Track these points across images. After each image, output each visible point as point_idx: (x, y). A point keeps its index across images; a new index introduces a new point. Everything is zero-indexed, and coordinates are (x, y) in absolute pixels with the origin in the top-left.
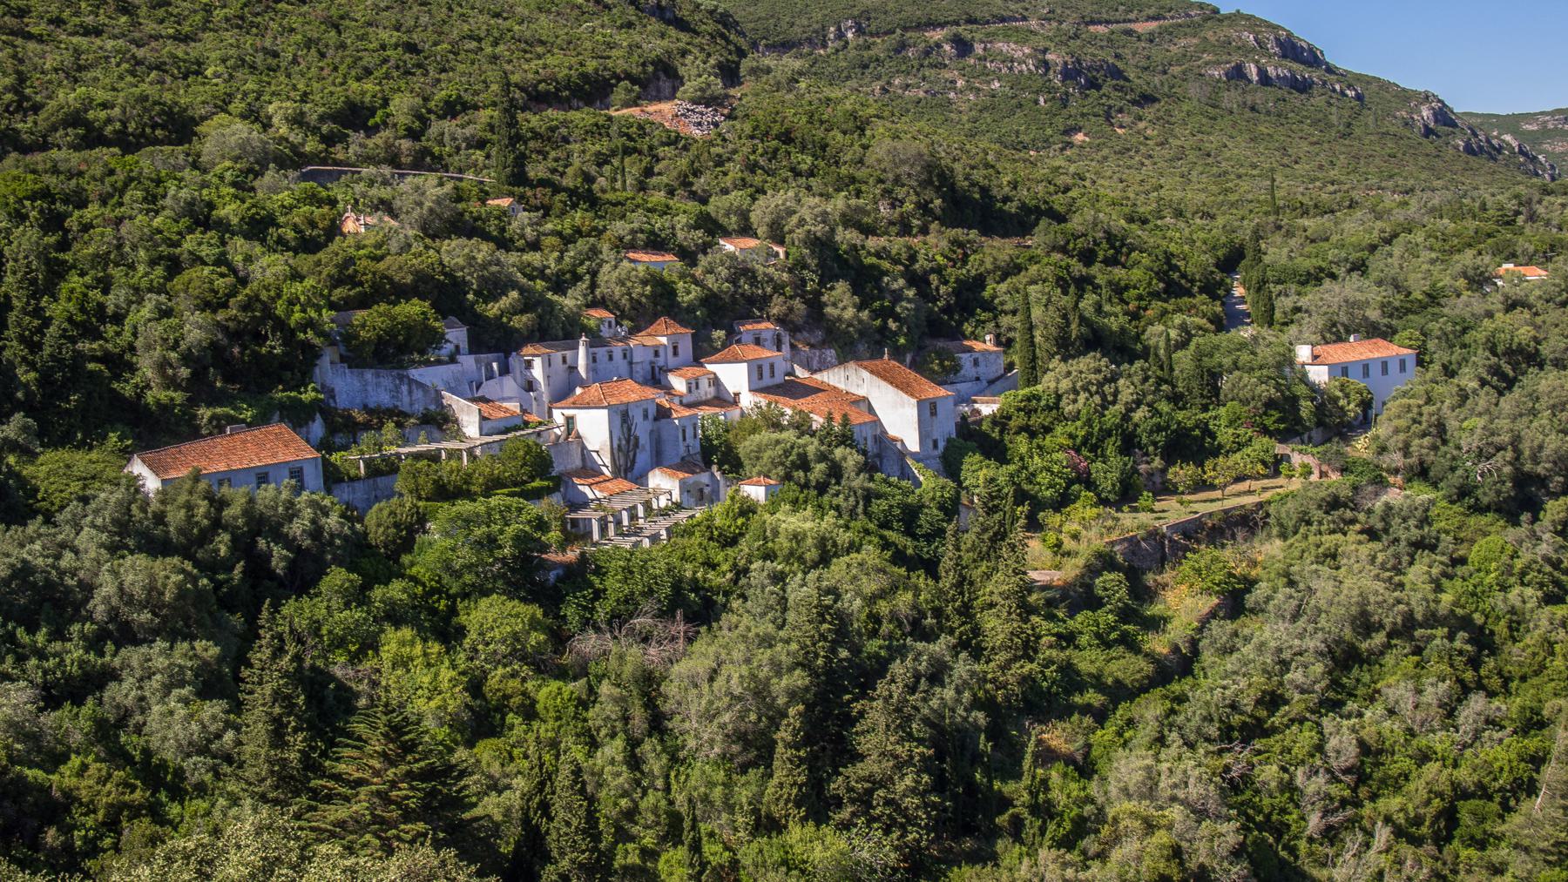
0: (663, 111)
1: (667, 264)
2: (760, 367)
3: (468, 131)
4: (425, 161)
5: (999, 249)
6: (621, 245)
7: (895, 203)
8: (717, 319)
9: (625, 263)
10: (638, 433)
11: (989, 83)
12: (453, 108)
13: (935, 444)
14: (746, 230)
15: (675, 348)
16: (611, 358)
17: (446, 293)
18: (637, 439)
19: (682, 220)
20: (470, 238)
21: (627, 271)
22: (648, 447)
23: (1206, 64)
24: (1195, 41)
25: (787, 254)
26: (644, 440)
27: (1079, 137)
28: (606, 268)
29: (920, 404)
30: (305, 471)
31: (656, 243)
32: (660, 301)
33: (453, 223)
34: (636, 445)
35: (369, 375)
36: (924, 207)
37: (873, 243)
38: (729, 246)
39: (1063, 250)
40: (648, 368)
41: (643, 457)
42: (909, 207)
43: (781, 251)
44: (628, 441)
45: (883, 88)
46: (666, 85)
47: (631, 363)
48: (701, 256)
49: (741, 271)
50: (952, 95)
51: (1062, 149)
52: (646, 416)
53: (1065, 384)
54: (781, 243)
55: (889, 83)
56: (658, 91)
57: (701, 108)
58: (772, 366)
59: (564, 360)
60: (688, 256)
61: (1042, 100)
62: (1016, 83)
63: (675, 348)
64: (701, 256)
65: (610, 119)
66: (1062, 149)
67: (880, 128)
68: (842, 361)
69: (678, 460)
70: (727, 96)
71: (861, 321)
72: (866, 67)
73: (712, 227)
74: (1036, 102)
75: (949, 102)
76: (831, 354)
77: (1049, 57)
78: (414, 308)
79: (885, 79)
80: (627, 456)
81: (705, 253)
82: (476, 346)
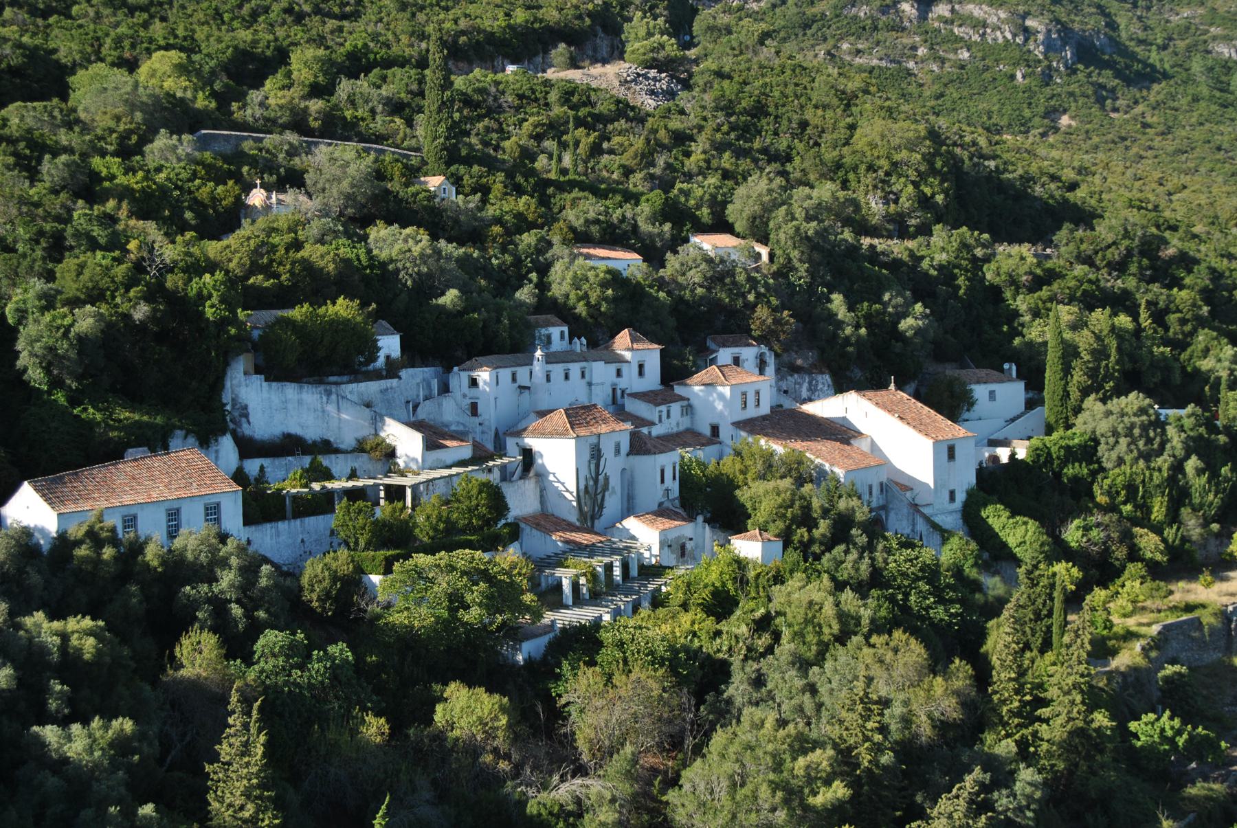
0: (606, 77)
1: (628, 262)
2: (744, 394)
3: (385, 91)
4: (336, 127)
5: (1013, 258)
6: (580, 237)
7: (890, 198)
8: (691, 329)
9: (580, 261)
10: (608, 471)
11: (955, 51)
12: (357, 64)
13: (952, 494)
14: (721, 225)
15: (641, 367)
16: (567, 377)
17: (374, 284)
18: (607, 479)
19: (645, 209)
20: (404, 226)
21: (579, 271)
22: (618, 489)
23: (1214, 38)
24: (1201, 11)
25: (772, 256)
26: (615, 482)
27: (1065, 120)
28: (558, 267)
29: (937, 443)
30: (240, 520)
31: (614, 236)
32: (628, 307)
33: (378, 204)
34: (606, 487)
35: (291, 390)
36: (925, 202)
37: (866, 241)
38: (707, 243)
39: (1088, 261)
40: (610, 391)
41: (612, 503)
42: (905, 203)
43: (764, 251)
44: (596, 481)
45: (829, 53)
46: (603, 43)
47: (590, 384)
48: (669, 255)
49: (720, 272)
50: (911, 65)
51: (1043, 135)
52: (618, 451)
53: (1103, 427)
54: (764, 240)
55: (836, 47)
56: (595, 50)
57: (653, 73)
58: (758, 393)
59: (514, 380)
60: (654, 255)
61: (1019, 75)
62: (988, 53)
63: (641, 367)
64: (669, 255)
65: (547, 83)
66: (1043, 135)
67: (867, 105)
68: (840, 387)
69: (655, 507)
70: (685, 58)
71: (859, 336)
72: (806, 26)
73: (682, 220)
74: (1012, 77)
75: (909, 73)
76: (825, 379)
77: (1030, 23)
78: (342, 308)
79: (831, 42)
80: (594, 500)
81: (676, 252)
82: (414, 354)
